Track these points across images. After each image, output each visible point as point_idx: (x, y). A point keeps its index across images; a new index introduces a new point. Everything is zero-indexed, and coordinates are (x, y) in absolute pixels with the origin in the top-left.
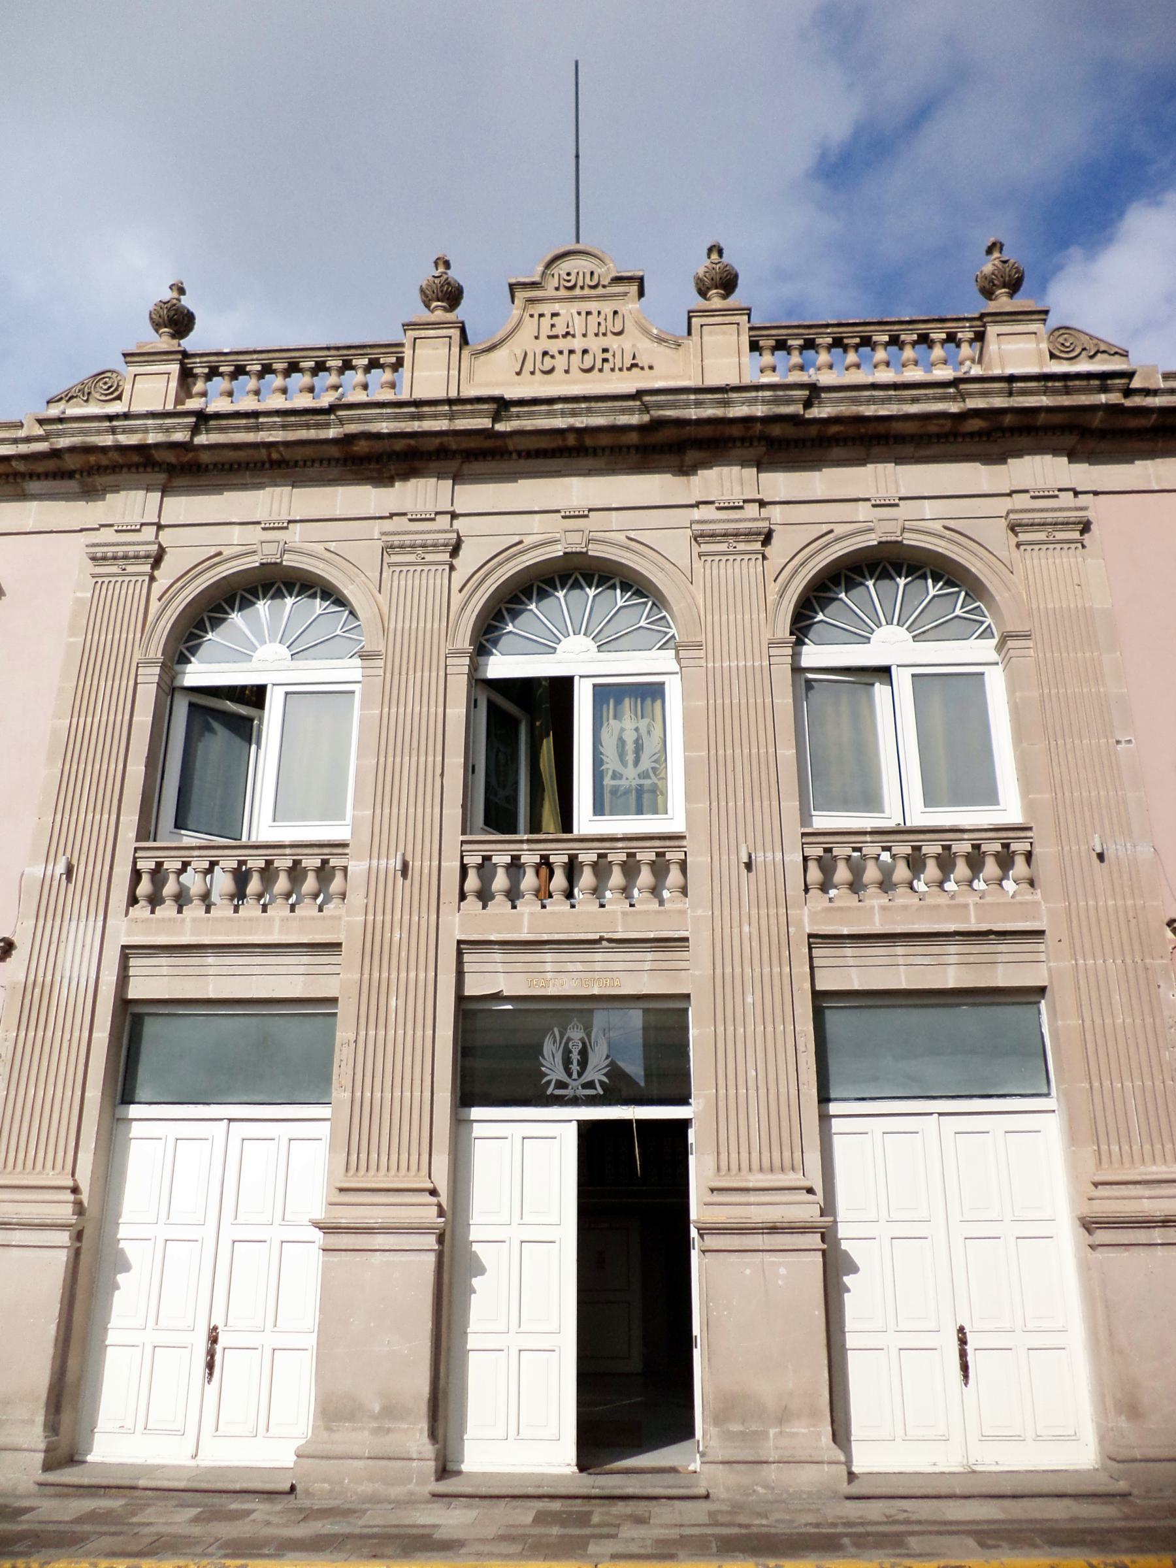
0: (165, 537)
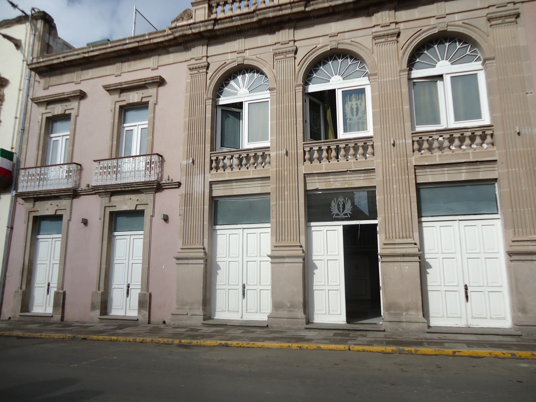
0: (209, 60)
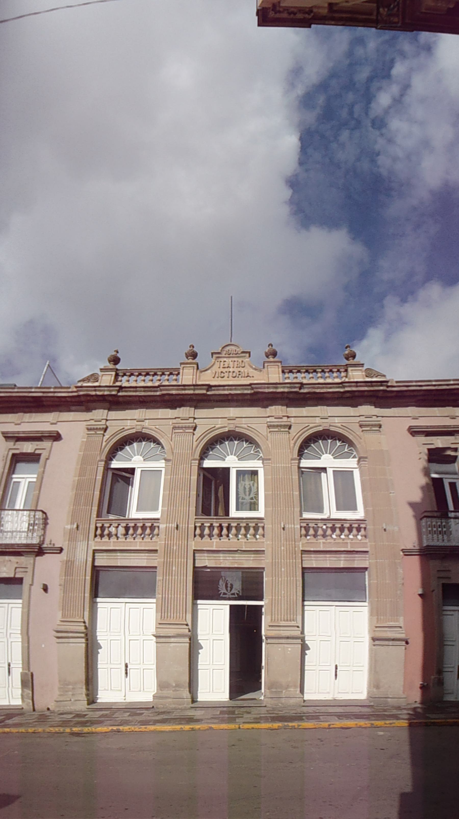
0: (108, 423)
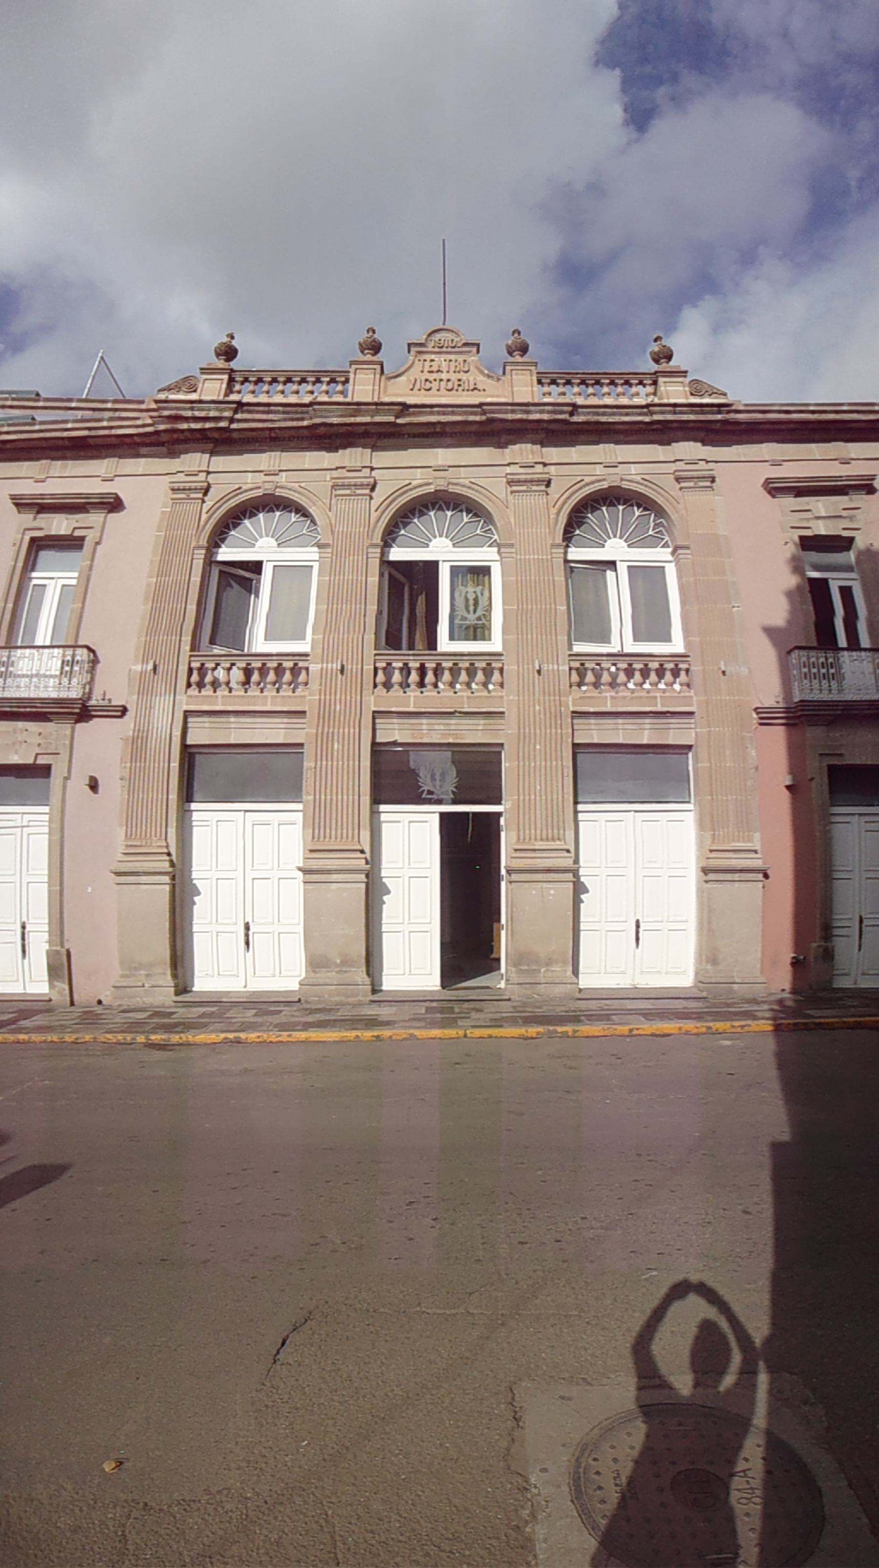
0: (211, 478)
